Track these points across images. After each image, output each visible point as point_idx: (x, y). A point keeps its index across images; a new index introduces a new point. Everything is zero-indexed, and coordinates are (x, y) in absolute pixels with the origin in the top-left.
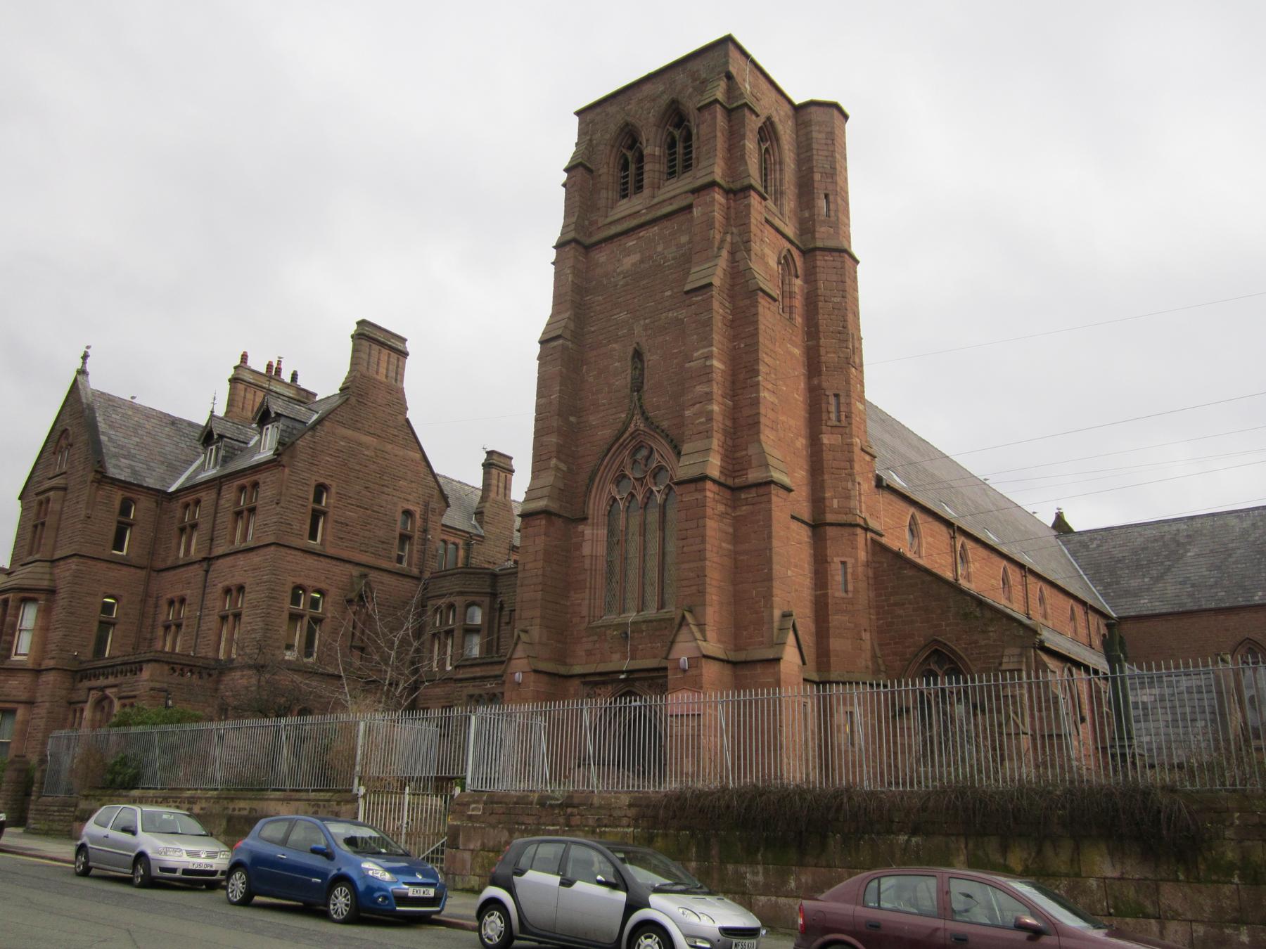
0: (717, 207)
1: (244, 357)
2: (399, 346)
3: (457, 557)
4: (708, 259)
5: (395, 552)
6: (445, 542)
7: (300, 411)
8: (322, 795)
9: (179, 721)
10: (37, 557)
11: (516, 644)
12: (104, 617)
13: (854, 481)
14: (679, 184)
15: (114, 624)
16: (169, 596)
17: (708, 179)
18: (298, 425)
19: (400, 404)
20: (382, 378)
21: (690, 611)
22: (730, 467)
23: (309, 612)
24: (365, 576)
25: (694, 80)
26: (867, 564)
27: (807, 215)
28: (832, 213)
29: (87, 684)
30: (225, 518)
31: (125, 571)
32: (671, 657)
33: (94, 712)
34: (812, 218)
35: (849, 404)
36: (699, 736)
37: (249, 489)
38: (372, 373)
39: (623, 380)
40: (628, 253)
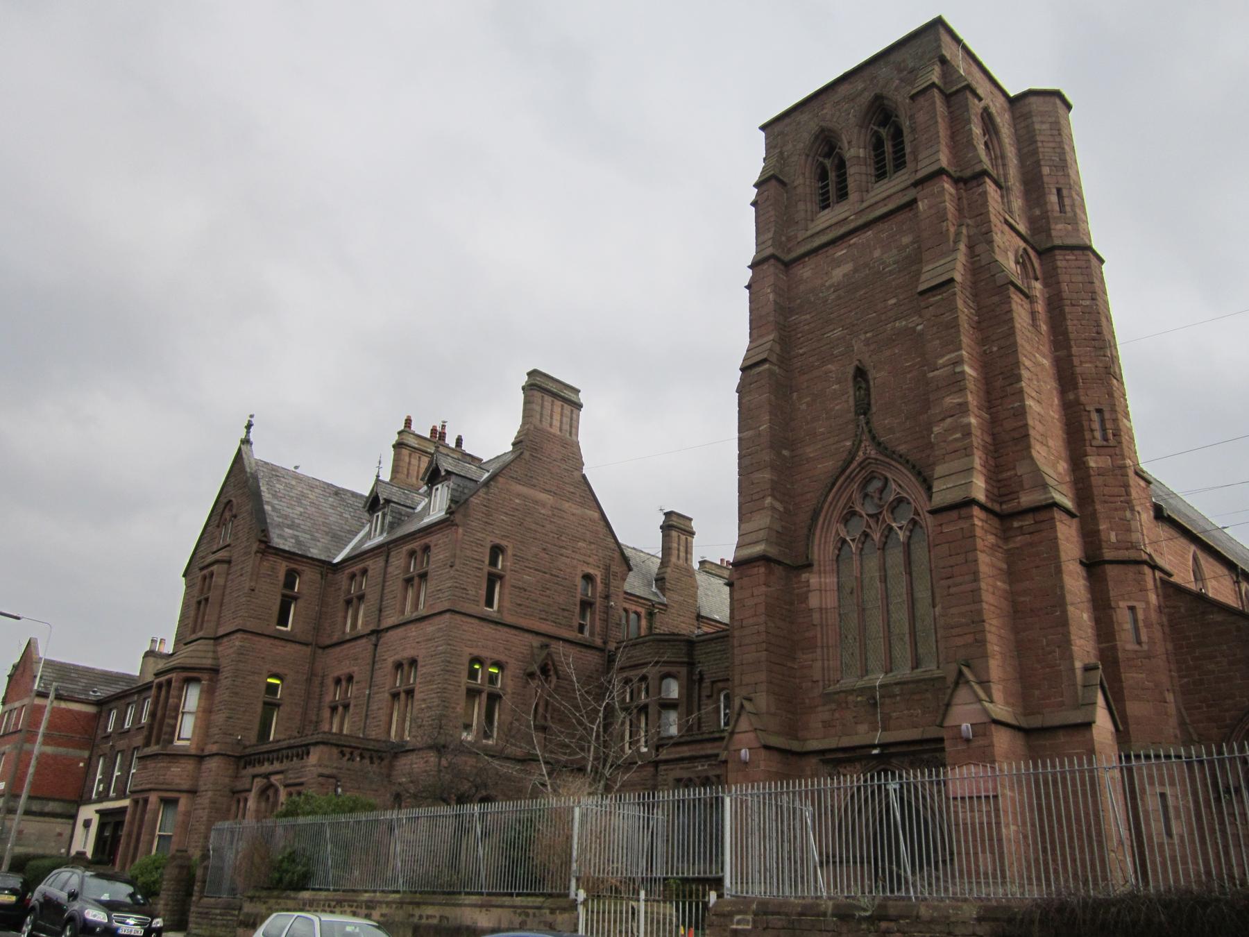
0: (947, 197)
1: (408, 422)
2: (572, 397)
3: (639, 628)
4: (943, 255)
5: (576, 621)
6: (626, 610)
7: (471, 470)
8: (530, 901)
9: (352, 810)
10: (200, 634)
11: (739, 715)
12: (269, 698)
13: (1132, 510)
14: (892, 184)
15: (278, 706)
16: (336, 674)
17: (934, 168)
18: (471, 485)
19: (574, 459)
20: (555, 430)
21: (968, 666)
22: (996, 491)
23: (487, 688)
24: (547, 646)
25: (900, 71)
26: (1160, 609)
27: (1038, 212)
28: (1068, 209)
29: (251, 771)
30: (395, 585)
31: (290, 648)
32: (946, 724)
33: (259, 802)
34: (1045, 216)
35: (1115, 420)
36: (998, 824)
37: (419, 553)
38: (545, 425)
39: (845, 403)
40: (838, 263)
